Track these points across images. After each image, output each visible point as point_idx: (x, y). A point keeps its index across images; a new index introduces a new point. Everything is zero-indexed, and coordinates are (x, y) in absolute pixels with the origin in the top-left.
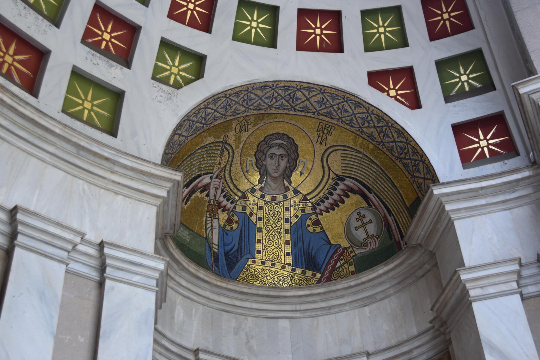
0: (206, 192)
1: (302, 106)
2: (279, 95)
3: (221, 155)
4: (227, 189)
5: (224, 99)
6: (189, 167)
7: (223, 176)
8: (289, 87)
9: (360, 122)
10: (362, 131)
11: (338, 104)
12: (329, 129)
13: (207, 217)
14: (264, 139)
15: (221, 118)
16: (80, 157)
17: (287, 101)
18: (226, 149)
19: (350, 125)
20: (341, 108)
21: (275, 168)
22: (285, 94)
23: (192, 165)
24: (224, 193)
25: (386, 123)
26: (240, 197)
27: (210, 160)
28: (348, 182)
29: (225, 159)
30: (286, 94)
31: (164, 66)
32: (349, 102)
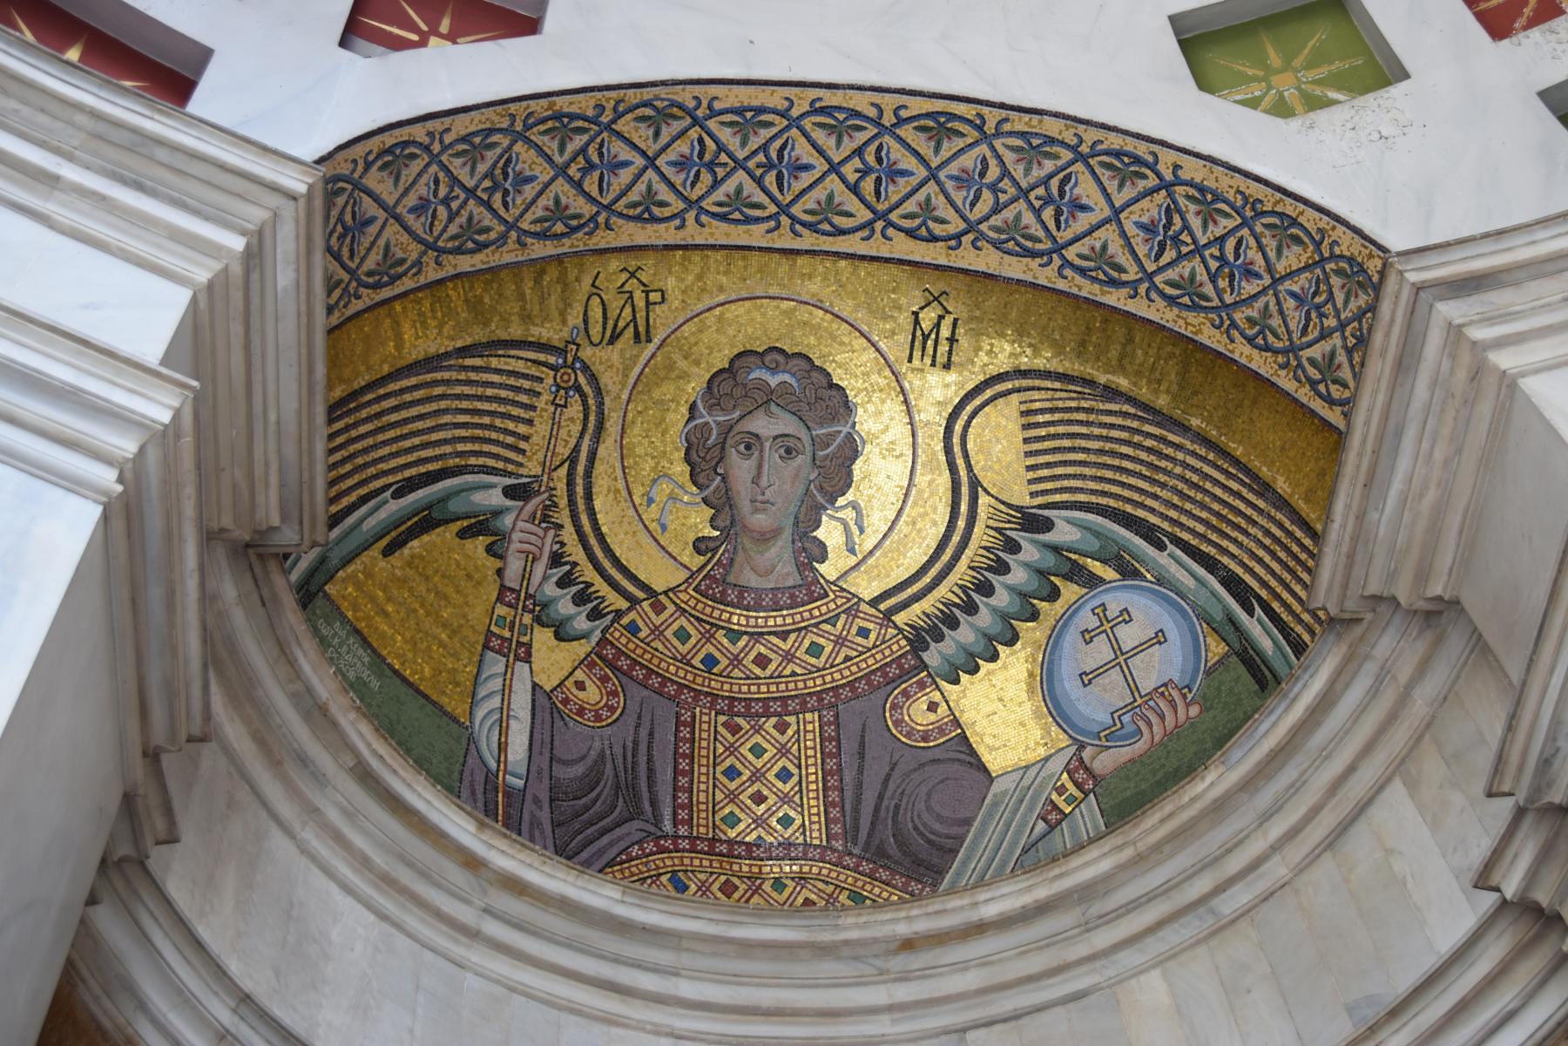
28: (1064, 532)
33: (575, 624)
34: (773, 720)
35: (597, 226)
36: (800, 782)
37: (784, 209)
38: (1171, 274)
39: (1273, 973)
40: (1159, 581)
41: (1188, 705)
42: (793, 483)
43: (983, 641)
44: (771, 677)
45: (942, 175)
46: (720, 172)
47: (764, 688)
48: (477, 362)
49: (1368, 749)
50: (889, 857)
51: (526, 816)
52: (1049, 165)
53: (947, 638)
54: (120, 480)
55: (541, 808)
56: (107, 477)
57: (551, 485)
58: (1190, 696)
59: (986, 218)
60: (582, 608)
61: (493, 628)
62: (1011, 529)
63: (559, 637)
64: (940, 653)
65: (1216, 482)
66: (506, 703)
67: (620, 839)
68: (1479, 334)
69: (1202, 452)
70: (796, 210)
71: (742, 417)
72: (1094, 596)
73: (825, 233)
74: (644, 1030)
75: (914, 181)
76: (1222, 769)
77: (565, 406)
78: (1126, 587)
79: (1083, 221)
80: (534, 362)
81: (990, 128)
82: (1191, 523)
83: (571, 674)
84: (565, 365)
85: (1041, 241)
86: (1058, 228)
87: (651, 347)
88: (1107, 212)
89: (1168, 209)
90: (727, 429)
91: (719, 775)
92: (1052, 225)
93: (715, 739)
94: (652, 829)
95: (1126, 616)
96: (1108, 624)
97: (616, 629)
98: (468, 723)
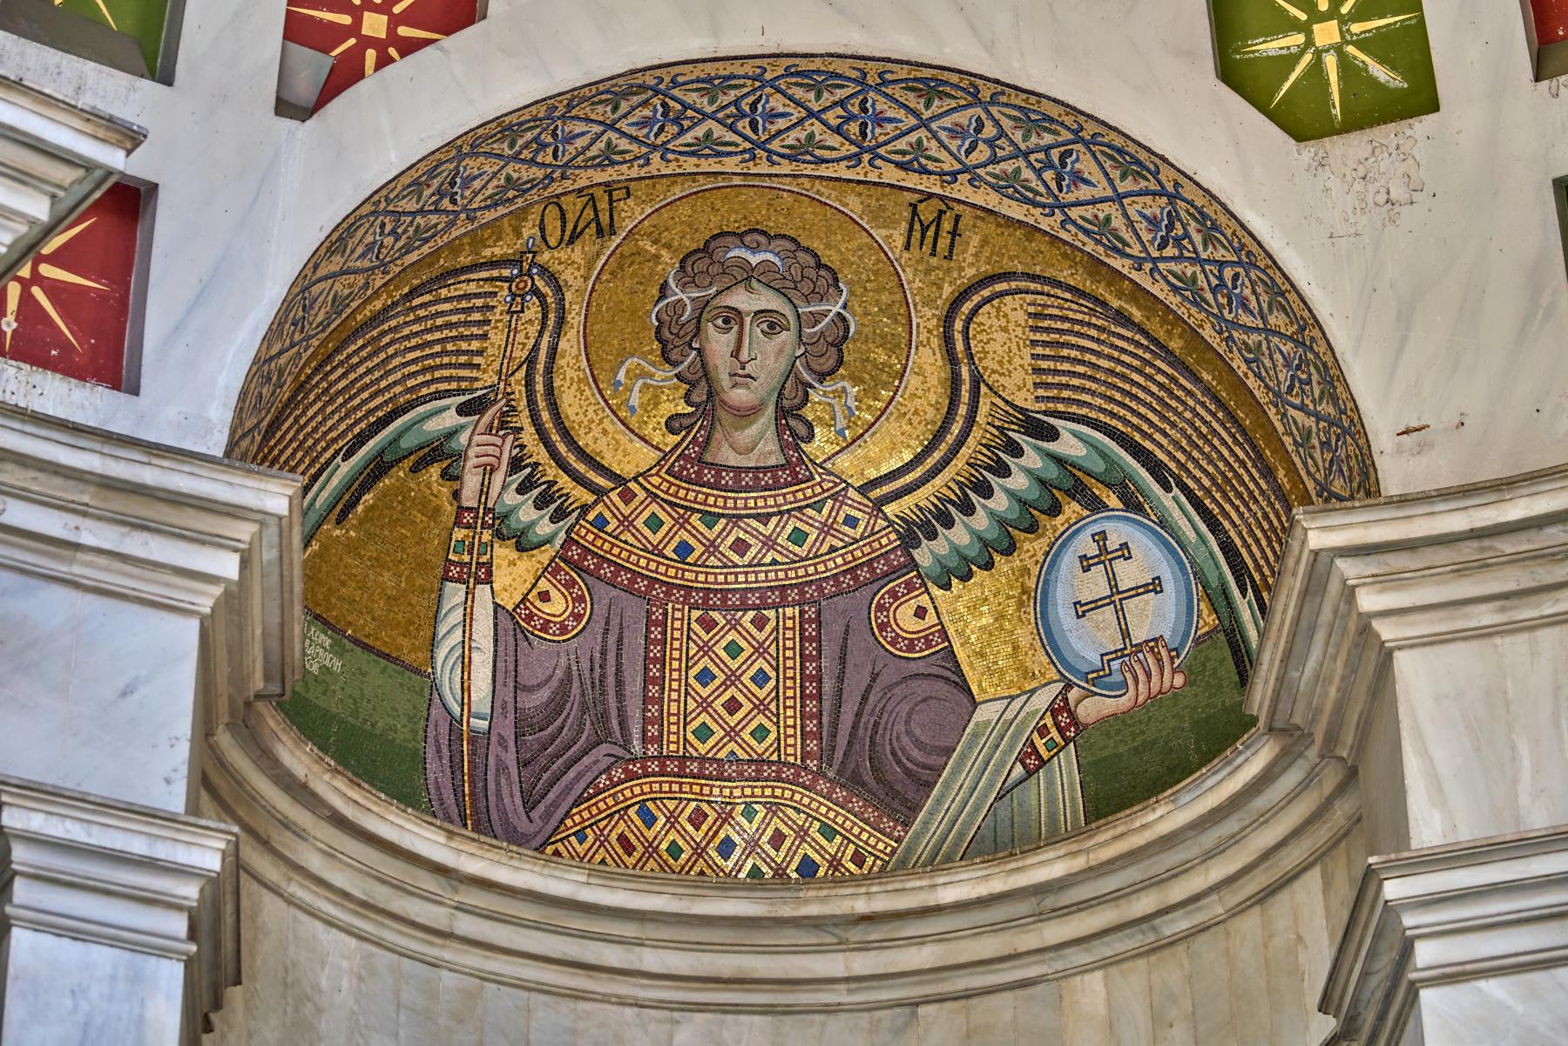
18: (536, 292)
28: (1069, 445)
33: (538, 530)
34: (751, 614)
36: (777, 687)
39: (1193, 1013)
40: (1162, 523)
41: (1174, 671)
42: (777, 359)
43: (978, 546)
44: (750, 565)
47: (741, 578)
48: (427, 298)
49: (1296, 833)
50: (863, 785)
51: (491, 760)
53: (940, 536)
54: (193, 935)
55: (506, 749)
56: (178, 925)
57: (509, 390)
58: (1177, 662)
59: (984, 165)
60: (544, 512)
61: (451, 557)
62: (1013, 430)
63: (520, 548)
64: (932, 552)
66: (467, 635)
67: (588, 768)
68: (1368, 601)
69: (1213, 407)
71: (719, 293)
72: (1095, 521)
74: (610, 1003)
76: (1171, 807)
77: (522, 311)
78: (1128, 519)
80: (486, 280)
82: (1198, 474)
83: (534, 585)
84: (521, 274)
85: (1042, 196)
87: (617, 240)
89: (1169, 213)
90: (703, 306)
91: (692, 681)
92: (1053, 186)
93: (689, 638)
94: (620, 752)
95: (1125, 551)
96: (1106, 556)
97: (582, 526)
98: (430, 670)
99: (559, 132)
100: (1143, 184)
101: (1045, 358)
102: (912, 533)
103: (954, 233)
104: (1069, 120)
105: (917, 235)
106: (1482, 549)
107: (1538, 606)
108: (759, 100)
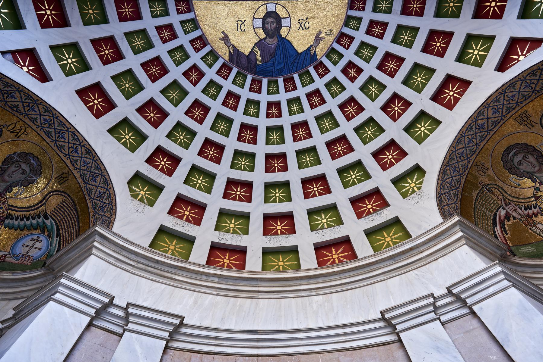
0: (511, 218)
1: (491, 125)
2: (471, 135)
3: (492, 193)
4: (521, 204)
5: (448, 168)
6: (482, 216)
7: (509, 202)
8: (470, 126)
9: (528, 90)
10: (538, 91)
11: (504, 100)
12: (525, 115)
13: (530, 229)
14: (503, 161)
15: (462, 177)
16: (398, 261)
17: (481, 132)
18: (490, 188)
19: (528, 99)
20: (508, 99)
21: (531, 166)
22: (473, 131)
23: (483, 214)
24: (523, 208)
25: (539, 70)
26: (535, 200)
27: (489, 202)
28: (48, 222)
29: (498, 193)
30: (474, 131)
31: (406, 189)
32: (507, 91)
35: (22, 115)
37: (56, 141)
38: (96, 201)
41: (30, 262)
43: (17, 226)
45: (83, 159)
46: (50, 127)
52: (97, 172)
59: (83, 170)
65: (74, 235)
70: (58, 143)
71: (21, 162)
73: (59, 149)
75: (78, 155)
79: (94, 183)
81: (95, 159)
82: (64, 238)
86: (90, 181)
87: (17, 139)
88: (97, 185)
92: (90, 180)
99: (33, 106)
100: (105, 186)
101: (58, 208)
102: (9, 217)
103: (65, 181)
104: (103, 170)
105: (59, 178)
106: (120, 251)
107: (122, 264)
108: (64, 133)
